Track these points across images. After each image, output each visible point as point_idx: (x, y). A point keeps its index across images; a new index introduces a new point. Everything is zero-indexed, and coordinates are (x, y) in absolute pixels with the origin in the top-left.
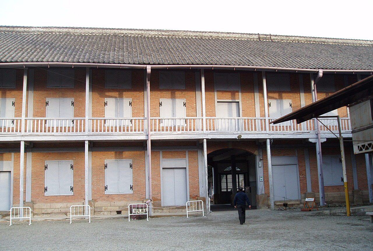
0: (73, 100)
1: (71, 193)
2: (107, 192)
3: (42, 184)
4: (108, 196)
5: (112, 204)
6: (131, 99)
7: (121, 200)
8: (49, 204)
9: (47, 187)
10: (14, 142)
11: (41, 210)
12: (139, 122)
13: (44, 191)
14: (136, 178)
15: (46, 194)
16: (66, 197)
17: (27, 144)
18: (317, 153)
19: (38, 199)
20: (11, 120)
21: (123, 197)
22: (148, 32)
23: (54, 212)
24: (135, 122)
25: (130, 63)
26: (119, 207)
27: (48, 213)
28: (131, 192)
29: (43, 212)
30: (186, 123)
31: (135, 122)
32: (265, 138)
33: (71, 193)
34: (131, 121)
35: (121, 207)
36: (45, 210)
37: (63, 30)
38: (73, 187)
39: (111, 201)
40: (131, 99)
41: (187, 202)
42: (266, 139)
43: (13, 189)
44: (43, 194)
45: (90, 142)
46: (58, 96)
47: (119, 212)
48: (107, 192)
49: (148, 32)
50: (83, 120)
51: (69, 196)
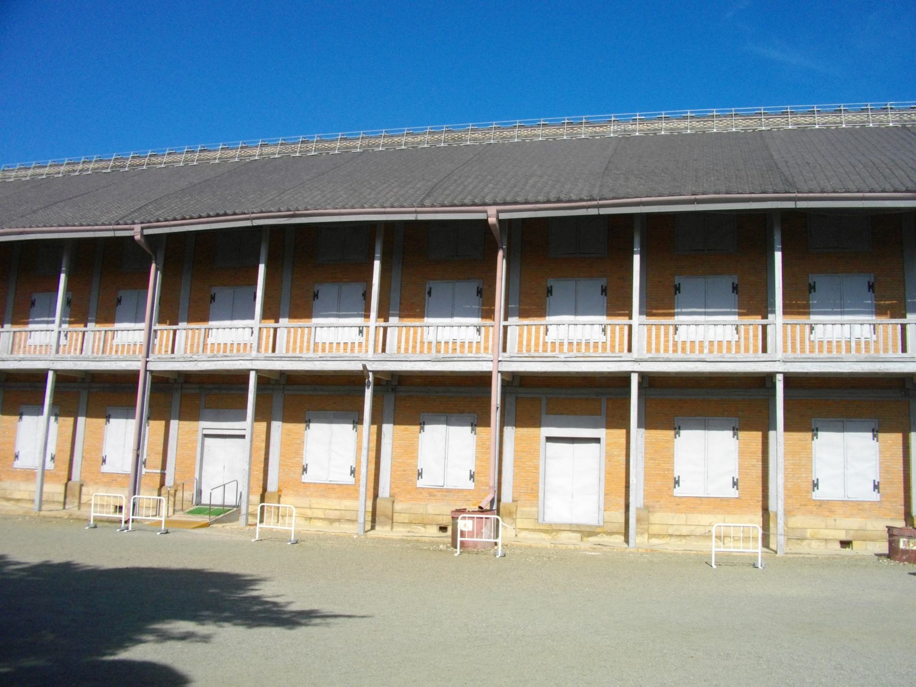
0: (735, 279)
1: (733, 493)
2: (817, 495)
3: (669, 470)
4: (821, 504)
5: (830, 522)
6: (872, 275)
7: (851, 515)
8: (683, 516)
9: (679, 477)
10: (420, 375)
11: (665, 527)
12: (658, 330)
13: (673, 486)
14: (889, 464)
15: (678, 492)
16: (721, 500)
17: (507, 379)
18: (493, 408)
19: (659, 502)
20: (358, 328)
21: (855, 507)
22: (877, 117)
23: (694, 533)
24: (613, 332)
25: (884, 188)
26: (847, 530)
27: (680, 536)
28: (875, 497)
29: (669, 533)
30: (875, 334)
31: (613, 332)
32: (246, 368)
33: (733, 493)
34: (737, 329)
35: (851, 532)
36: (676, 527)
37: (679, 126)
38: (474, 472)
39: (828, 516)
40: (872, 275)
41: (293, 507)
42: (48, 370)
43: (605, 477)
44: (810, 494)
45: (643, 376)
46: (701, 272)
47: (845, 544)
48: (817, 495)
49: (877, 117)
50: (292, 329)
51: (728, 499)
